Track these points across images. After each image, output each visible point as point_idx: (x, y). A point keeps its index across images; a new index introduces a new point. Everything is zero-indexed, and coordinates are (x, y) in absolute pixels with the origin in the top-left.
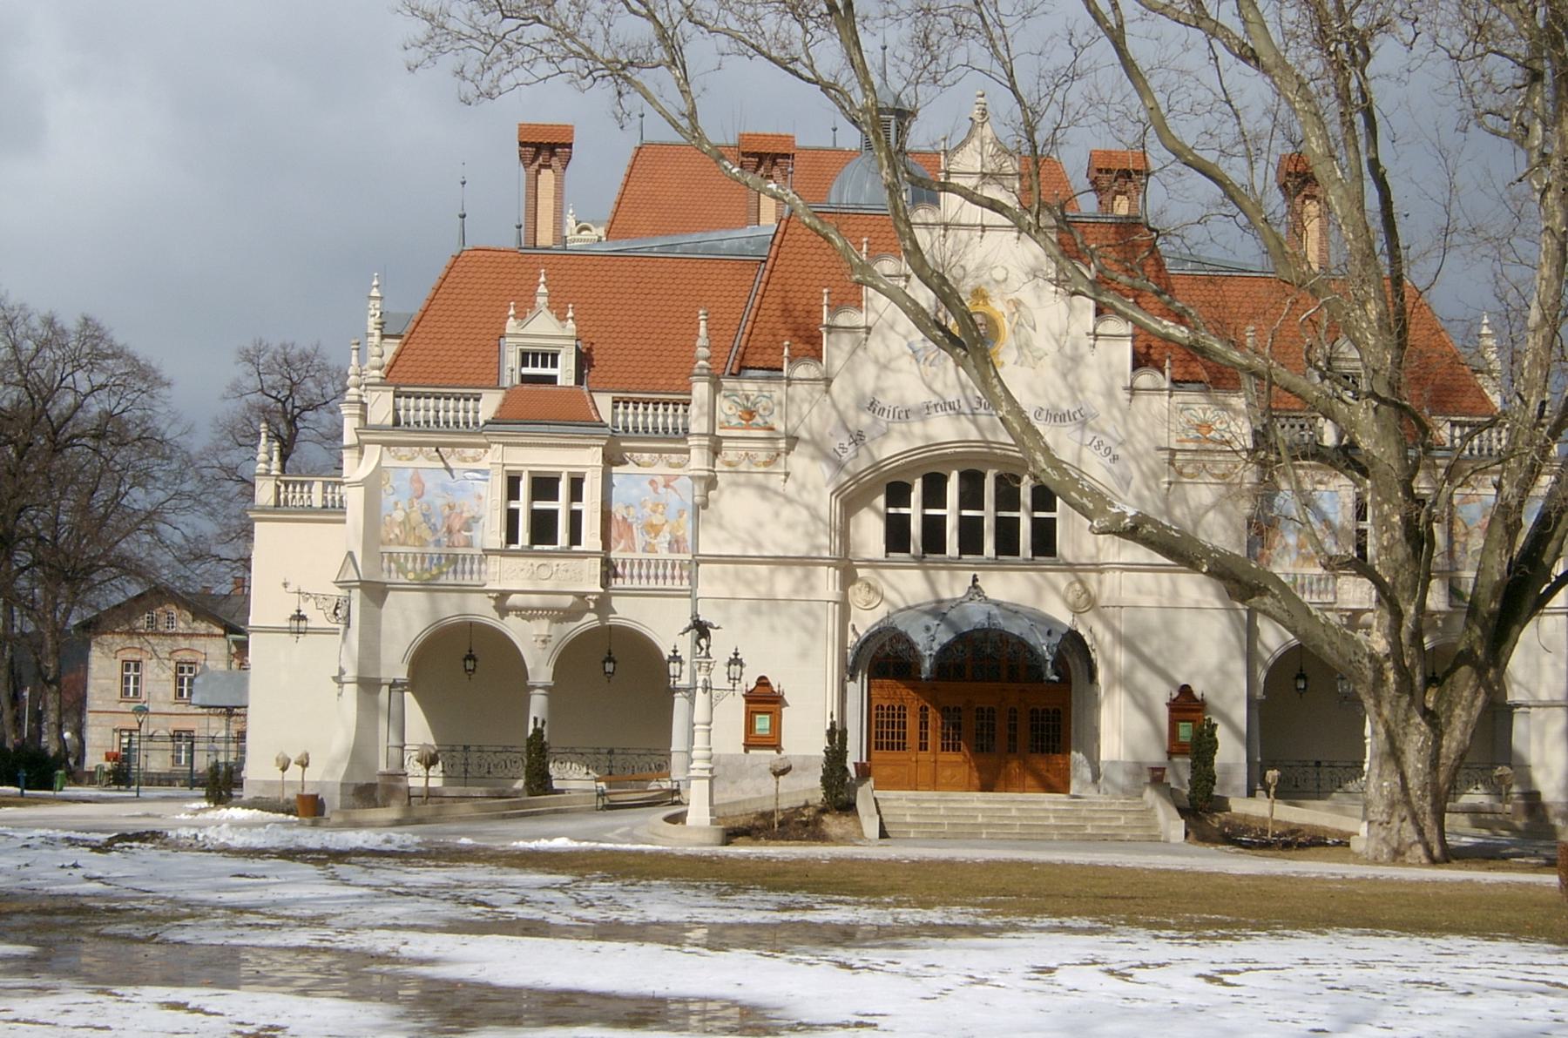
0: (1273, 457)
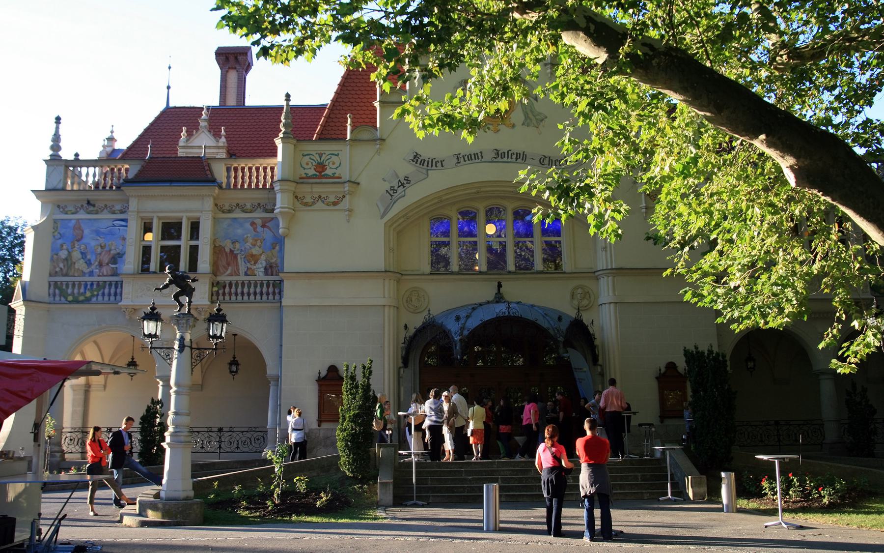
0: (579, 291)
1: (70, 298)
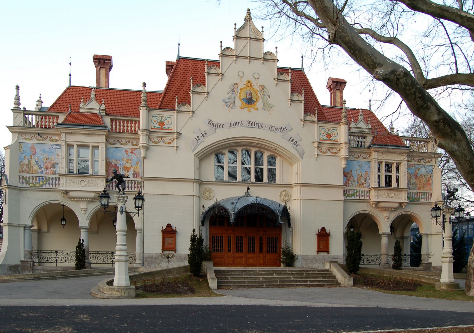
0: (284, 193)
1: (31, 185)
